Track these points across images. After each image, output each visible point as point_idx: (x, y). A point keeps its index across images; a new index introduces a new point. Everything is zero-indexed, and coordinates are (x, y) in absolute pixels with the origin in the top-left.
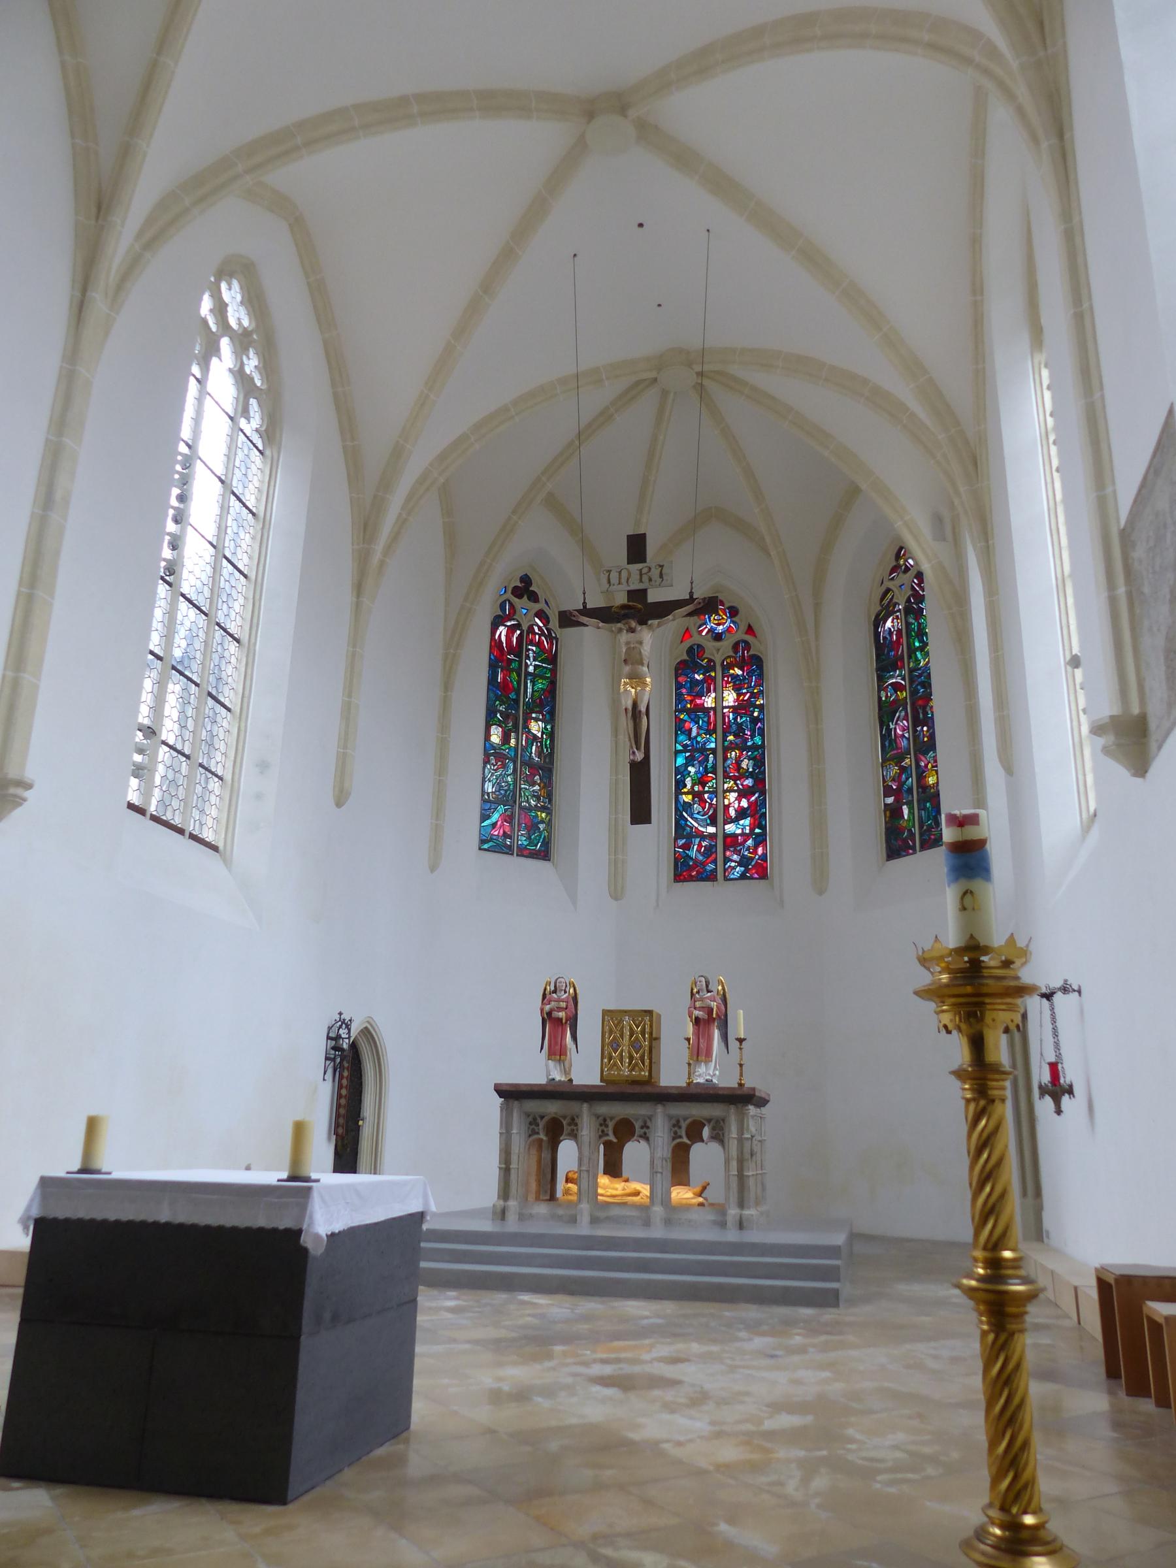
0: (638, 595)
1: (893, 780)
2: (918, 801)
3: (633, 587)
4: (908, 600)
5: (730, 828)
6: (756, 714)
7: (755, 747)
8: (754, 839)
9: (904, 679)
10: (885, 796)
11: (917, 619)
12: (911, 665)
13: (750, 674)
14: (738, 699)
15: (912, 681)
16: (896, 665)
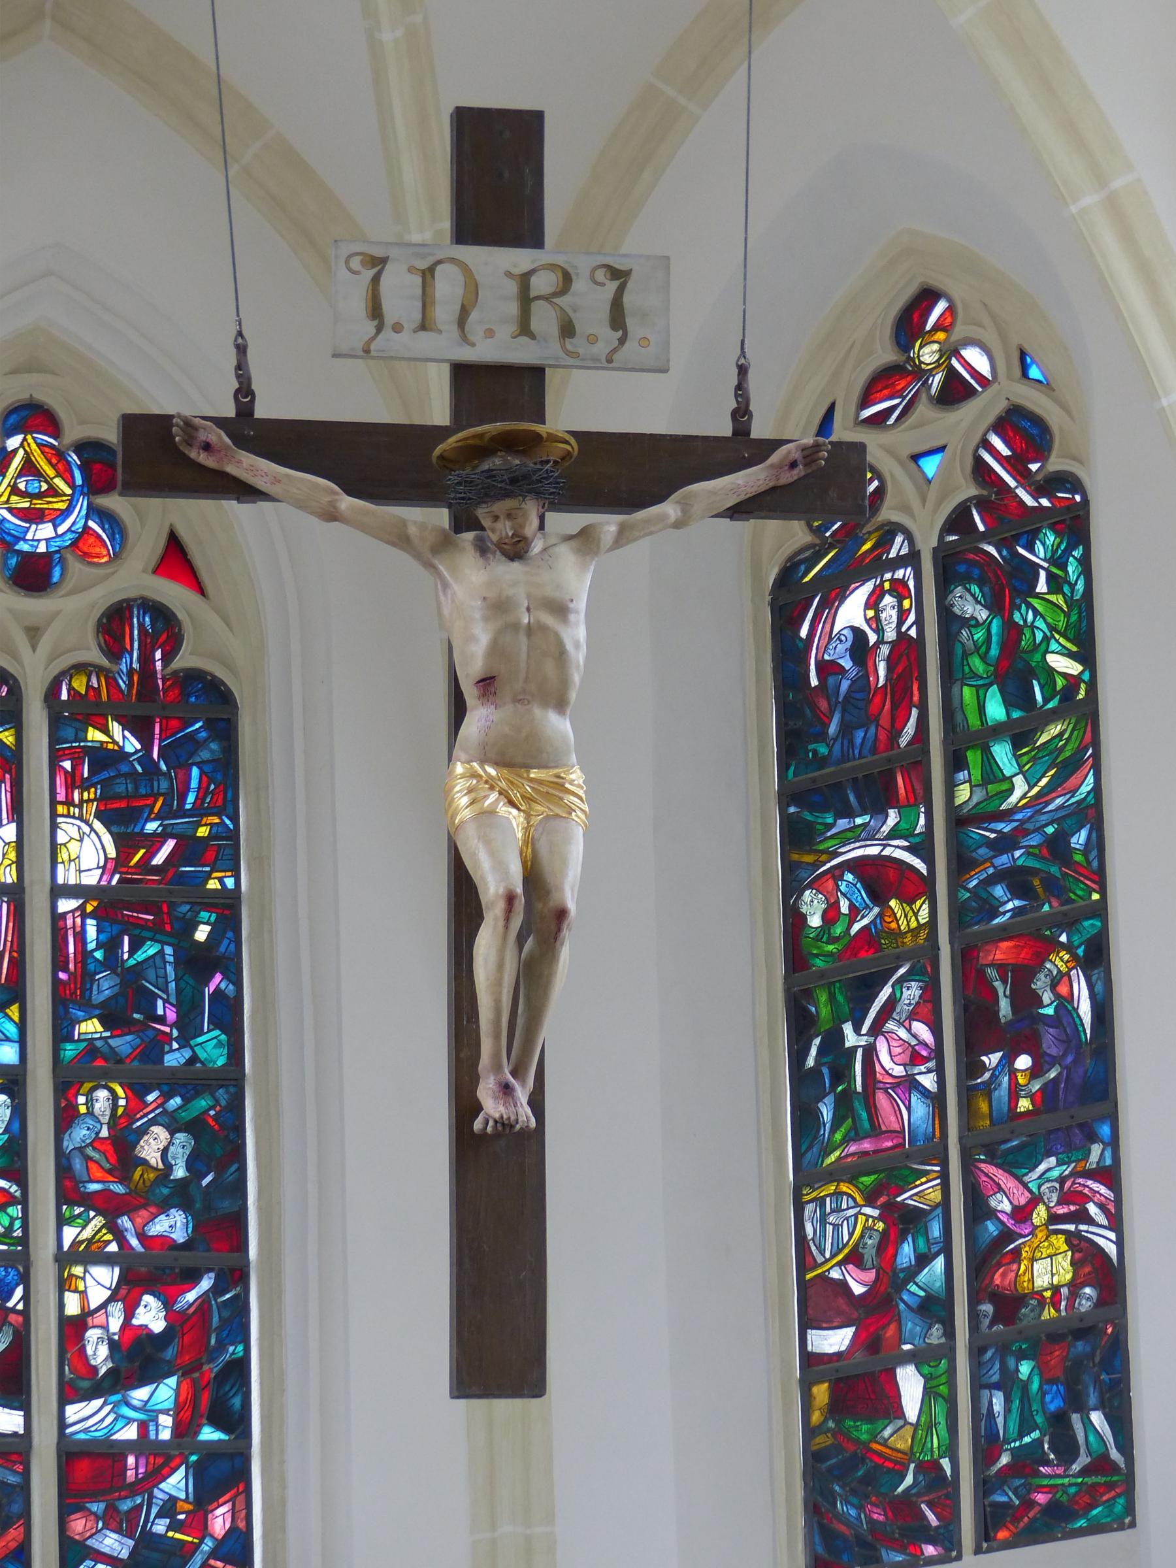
0: (497, 391)
1: (855, 1258)
2: (977, 1352)
3: (485, 351)
4: (959, 521)
5: (88, 1416)
6: (202, 934)
7: (194, 1080)
8: (199, 1473)
9: (922, 848)
10: (807, 1323)
11: (998, 604)
12: (963, 794)
13: (180, 754)
14: (120, 862)
15: (961, 863)
16: (880, 787)
